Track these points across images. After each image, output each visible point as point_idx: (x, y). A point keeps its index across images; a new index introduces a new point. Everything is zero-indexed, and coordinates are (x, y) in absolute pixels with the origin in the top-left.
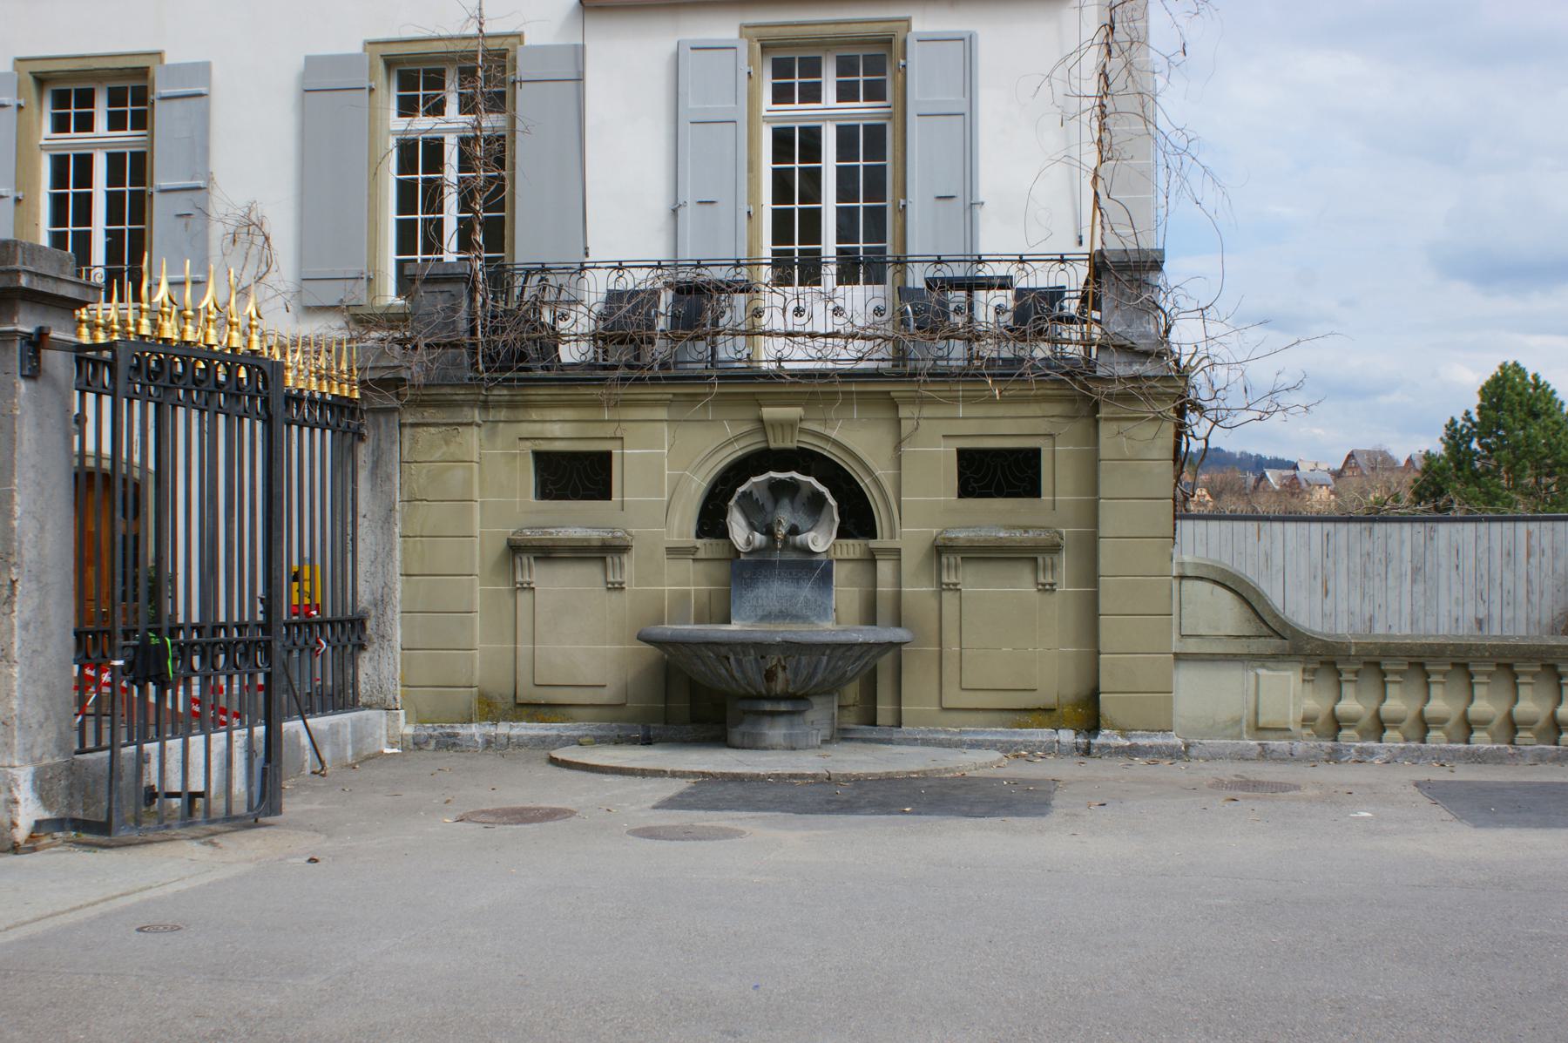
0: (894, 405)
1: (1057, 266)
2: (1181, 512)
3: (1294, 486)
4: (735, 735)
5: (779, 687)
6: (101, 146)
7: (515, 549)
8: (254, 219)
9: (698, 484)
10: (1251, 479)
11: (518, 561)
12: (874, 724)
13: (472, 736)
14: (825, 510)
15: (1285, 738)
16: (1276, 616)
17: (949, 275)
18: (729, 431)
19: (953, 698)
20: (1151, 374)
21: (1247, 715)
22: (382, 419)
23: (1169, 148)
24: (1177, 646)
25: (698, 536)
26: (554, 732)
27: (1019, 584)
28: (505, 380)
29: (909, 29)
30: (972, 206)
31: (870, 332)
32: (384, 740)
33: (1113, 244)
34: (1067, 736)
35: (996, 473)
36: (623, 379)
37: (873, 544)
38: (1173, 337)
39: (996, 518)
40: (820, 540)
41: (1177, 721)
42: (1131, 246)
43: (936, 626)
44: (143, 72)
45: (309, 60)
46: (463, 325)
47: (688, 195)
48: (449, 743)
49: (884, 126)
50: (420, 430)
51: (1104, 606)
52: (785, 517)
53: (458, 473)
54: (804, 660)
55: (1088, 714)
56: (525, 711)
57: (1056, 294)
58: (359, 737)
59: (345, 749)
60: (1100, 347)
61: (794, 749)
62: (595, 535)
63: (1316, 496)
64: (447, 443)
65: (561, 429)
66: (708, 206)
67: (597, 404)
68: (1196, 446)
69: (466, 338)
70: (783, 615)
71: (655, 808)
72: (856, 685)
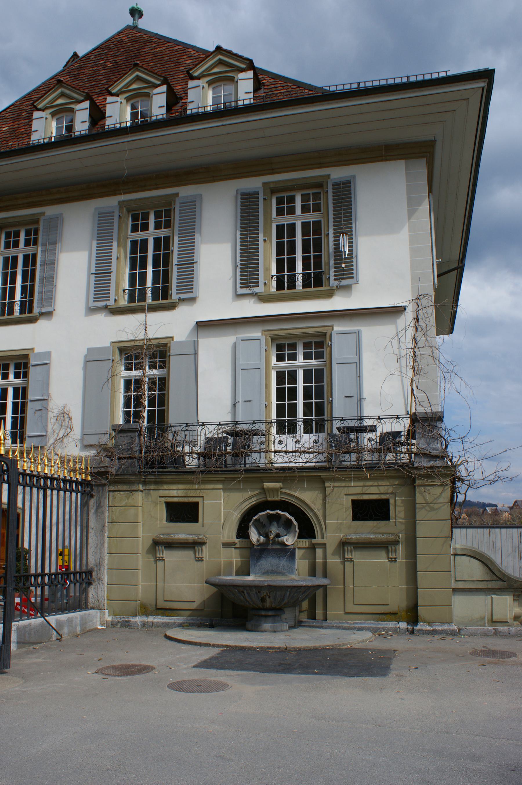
0: (322, 481)
1: (395, 421)
2: (455, 524)
3: (496, 512)
4: (249, 625)
5: (268, 604)
6: (10, 385)
7: (156, 543)
8: (65, 410)
9: (236, 516)
10: (481, 510)
11: (157, 548)
12: (314, 619)
13: (136, 622)
14: (292, 527)
15: (506, 626)
16: (500, 571)
17: (347, 425)
18: (250, 494)
19: (350, 608)
20: (439, 465)
21: (488, 615)
22: (100, 488)
23: (445, 370)
24: (453, 585)
25: (237, 538)
26: (172, 621)
27: (380, 558)
28: (153, 472)
29: (333, 329)
30: (360, 400)
31: (312, 450)
32: (98, 623)
33: (420, 410)
34: (403, 625)
35: (368, 510)
36: (202, 472)
37: (314, 541)
38: (449, 449)
39: (368, 530)
40: (289, 540)
41: (454, 618)
42: (428, 410)
43: (342, 576)
44: (26, 356)
45: (89, 350)
46: (136, 448)
47: (240, 398)
48: (126, 625)
49: (323, 369)
50: (116, 493)
51: (420, 566)
52: (274, 530)
53: (132, 511)
54: (278, 593)
55: (413, 615)
56: (160, 611)
57: (398, 434)
58: (84, 622)
59: (76, 628)
60: (416, 454)
61: (275, 632)
62: (190, 537)
63: (504, 516)
64: (128, 499)
65: (176, 493)
66: (248, 403)
67: (191, 482)
68: (461, 498)
69: (137, 454)
70: (273, 572)
71: (195, 667)
72: (304, 604)
